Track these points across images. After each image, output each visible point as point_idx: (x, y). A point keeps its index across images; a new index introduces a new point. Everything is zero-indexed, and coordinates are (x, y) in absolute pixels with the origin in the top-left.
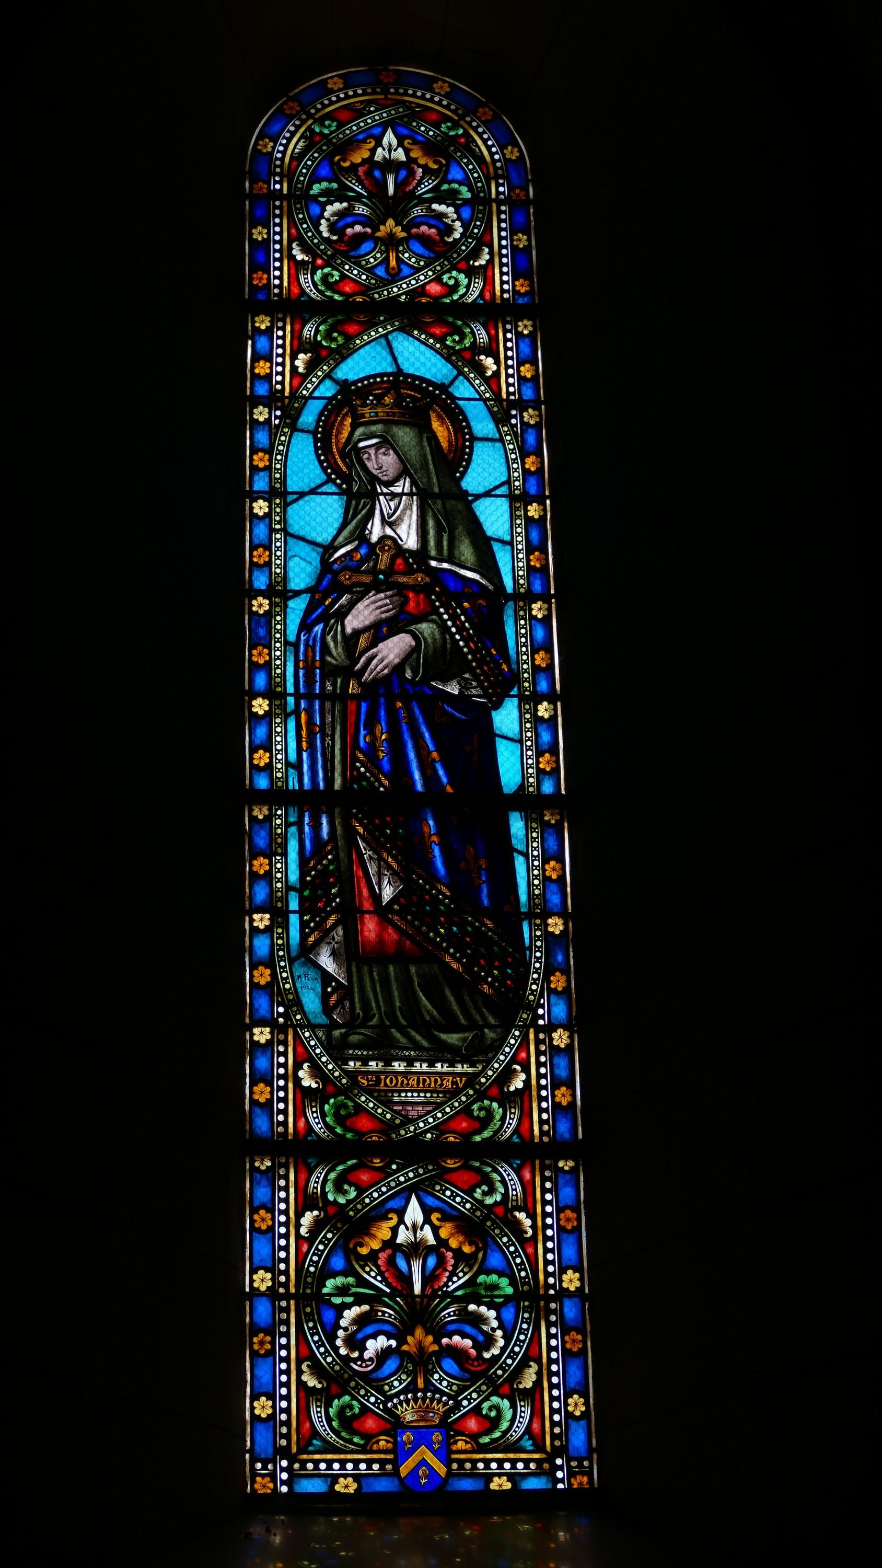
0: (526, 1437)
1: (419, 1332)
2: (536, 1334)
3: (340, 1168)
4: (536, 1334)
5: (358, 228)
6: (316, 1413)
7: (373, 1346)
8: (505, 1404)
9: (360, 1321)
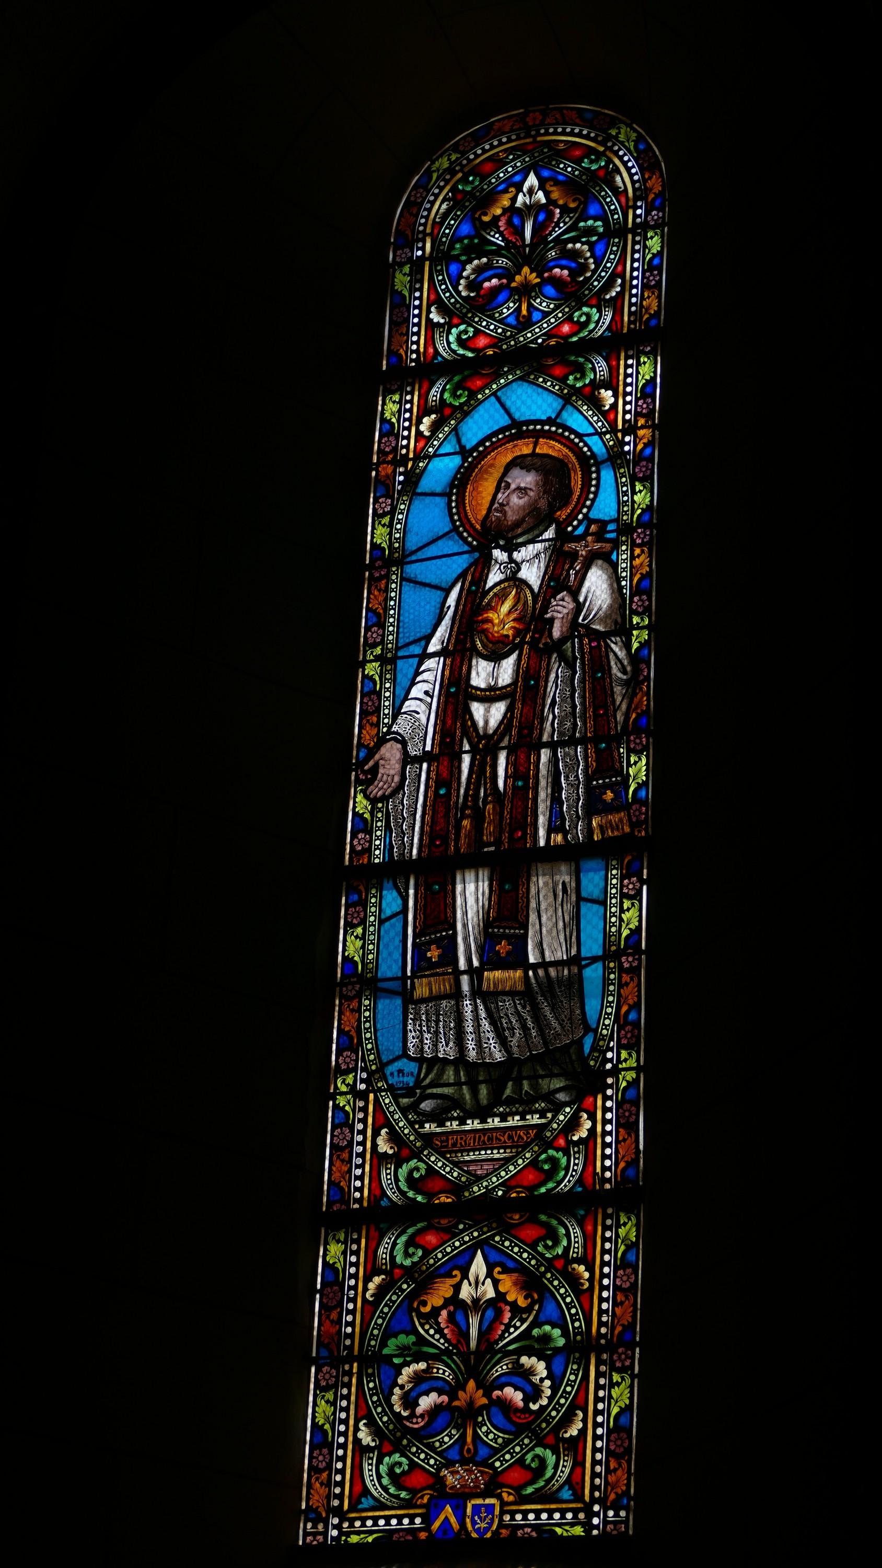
0: (567, 1487)
1: (526, 270)
2: (584, 1384)
3: (410, 1231)
4: (584, 1384)
5: (495, 281)
6: (385, 1177)
7: (425, 1403)
8: (551, 1459)
9: (418, 1378)
